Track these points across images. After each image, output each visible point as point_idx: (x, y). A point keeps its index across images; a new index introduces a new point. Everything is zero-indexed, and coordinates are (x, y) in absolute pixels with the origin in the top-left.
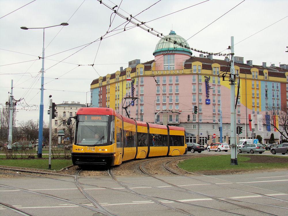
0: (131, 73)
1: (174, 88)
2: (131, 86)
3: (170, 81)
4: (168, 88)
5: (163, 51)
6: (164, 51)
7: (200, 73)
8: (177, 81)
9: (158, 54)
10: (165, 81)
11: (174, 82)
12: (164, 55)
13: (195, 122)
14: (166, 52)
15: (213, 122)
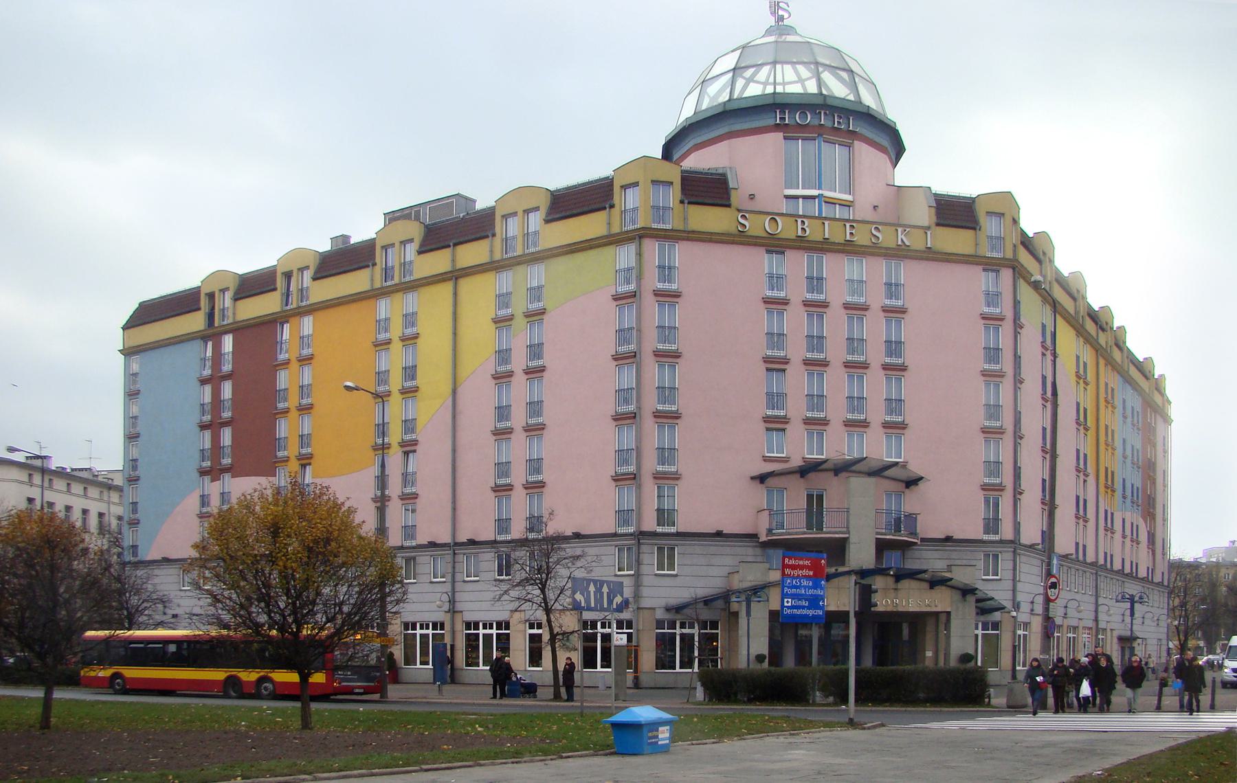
7: (1000, 255)
8: (892, 288)
10: (815, 282)
11: (876, 298)
14: (803, 114)
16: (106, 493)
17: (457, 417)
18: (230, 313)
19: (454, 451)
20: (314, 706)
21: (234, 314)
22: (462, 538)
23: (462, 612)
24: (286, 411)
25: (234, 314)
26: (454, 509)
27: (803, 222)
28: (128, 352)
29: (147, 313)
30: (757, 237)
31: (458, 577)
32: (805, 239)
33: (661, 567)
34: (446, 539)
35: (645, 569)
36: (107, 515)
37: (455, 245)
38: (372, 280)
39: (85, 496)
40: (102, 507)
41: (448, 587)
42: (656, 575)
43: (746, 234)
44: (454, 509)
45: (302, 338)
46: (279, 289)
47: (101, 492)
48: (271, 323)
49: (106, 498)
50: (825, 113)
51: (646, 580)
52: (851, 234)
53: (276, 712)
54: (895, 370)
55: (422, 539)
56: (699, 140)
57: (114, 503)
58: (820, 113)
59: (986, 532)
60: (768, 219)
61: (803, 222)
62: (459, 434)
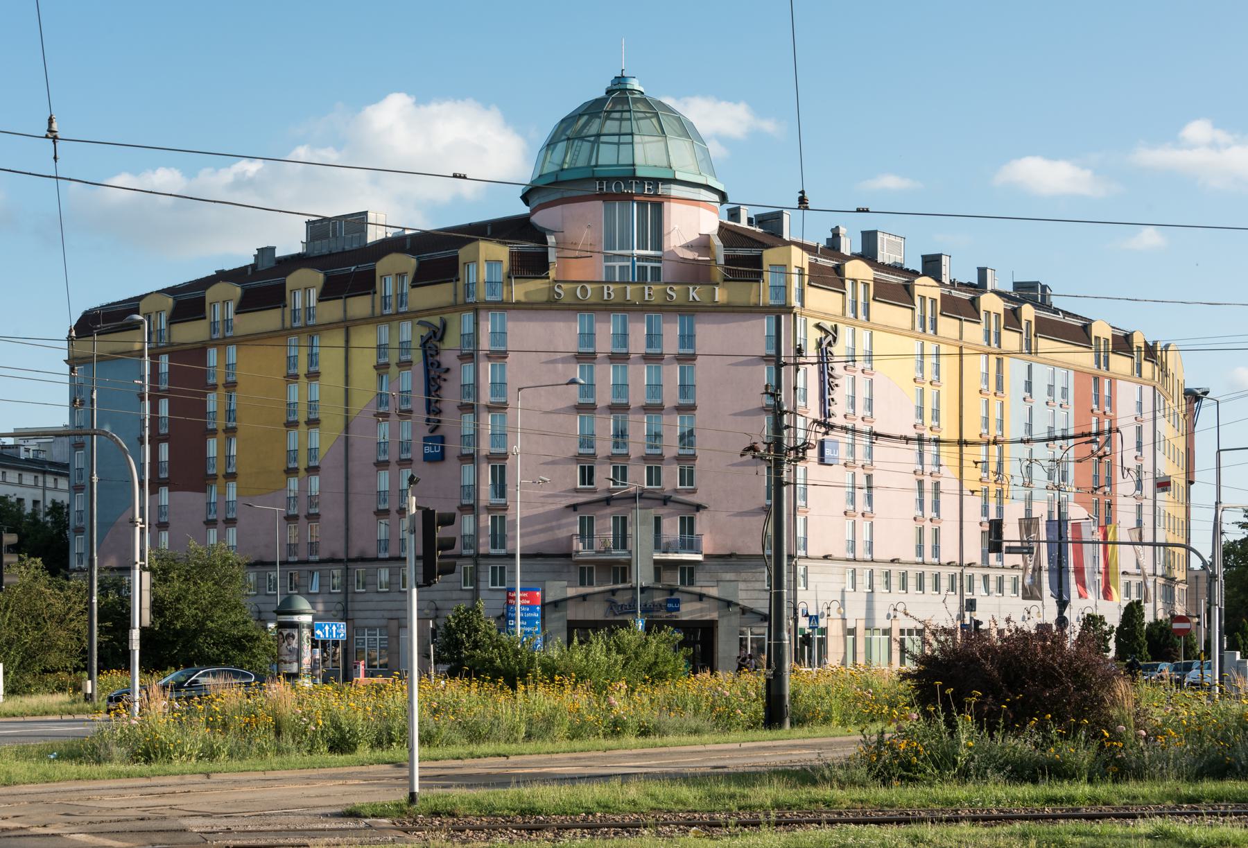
0: (413, 287)
1: (672, 374)
2: (417, 356)
3: (653, 338)
4: (640, 376)
5: (601, 180)
6: (609, 180)
9: (566, 195)
12: (606, 197)
13: (503, 552)
15: (493, 552)
16: (40, 478)
17: (349, 449)
18: (165, 334)
19: (347, 478)
20: (1057, 544)
21: (169, 336)
22: (354, 554)
23: (352, 619)
24: (215, 477)
25: (169, 336)
26: (347, 529)
27: (608, 289)
28: (73, 362)
29: (89, 324)
30: (570, 304)
31: (350, 588)
32: (610, 303)
33: (494, 583)
34: (342, 555)
35: (482, 585)
36: (42, 502)
37: (346, 297)
38: (283, 320)
39: (20, 484)
40: (38, 494)
41: (341, 598)
42: (490, 590)
43: (560, 302)
44: (347, 529)
45: (227, 366)
46: (208, 318)
47: (36, 477)
48: (198, 352)
49: (40, 484)
50: (636, 183)
51: (483, 594)
52: (650, 295)
53: (706, 615)
54: (686, 409)
55: (324, 554)
56: (543, 201)
57: (50, 489)
58: (632, 182)
59: (494, 546)
60: (579, 288)
61: (608, 289)
62: (350, 464)
